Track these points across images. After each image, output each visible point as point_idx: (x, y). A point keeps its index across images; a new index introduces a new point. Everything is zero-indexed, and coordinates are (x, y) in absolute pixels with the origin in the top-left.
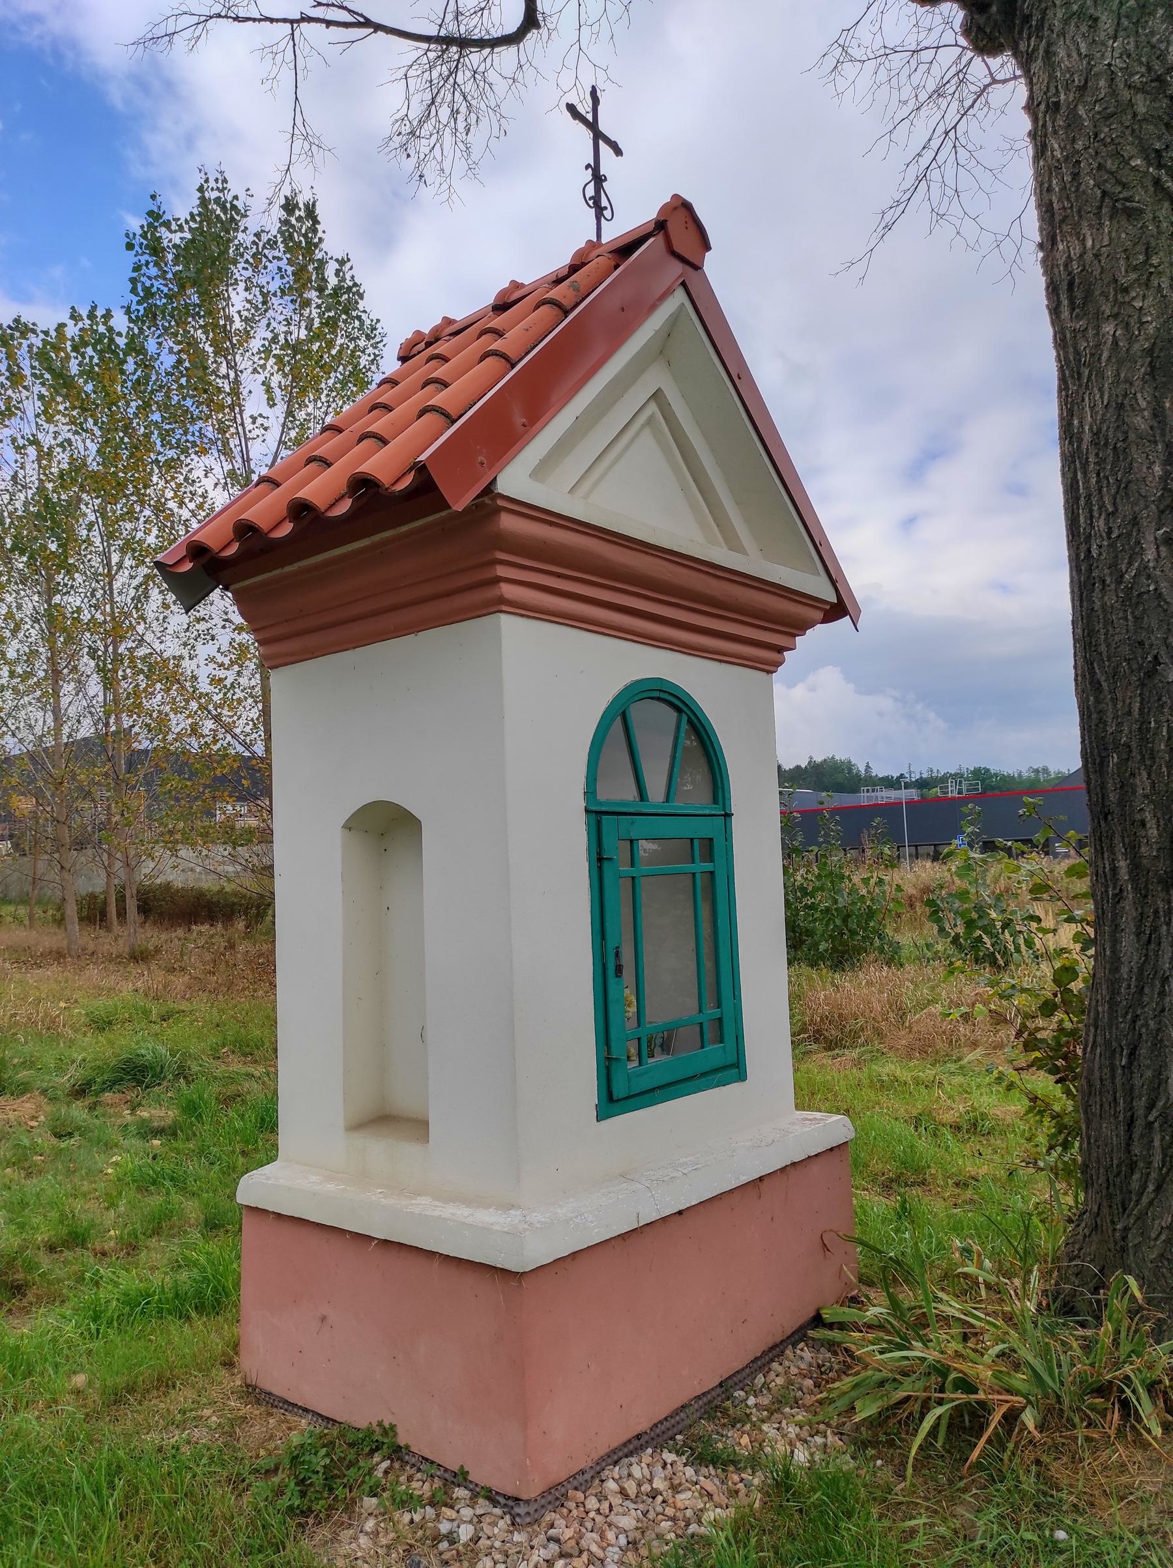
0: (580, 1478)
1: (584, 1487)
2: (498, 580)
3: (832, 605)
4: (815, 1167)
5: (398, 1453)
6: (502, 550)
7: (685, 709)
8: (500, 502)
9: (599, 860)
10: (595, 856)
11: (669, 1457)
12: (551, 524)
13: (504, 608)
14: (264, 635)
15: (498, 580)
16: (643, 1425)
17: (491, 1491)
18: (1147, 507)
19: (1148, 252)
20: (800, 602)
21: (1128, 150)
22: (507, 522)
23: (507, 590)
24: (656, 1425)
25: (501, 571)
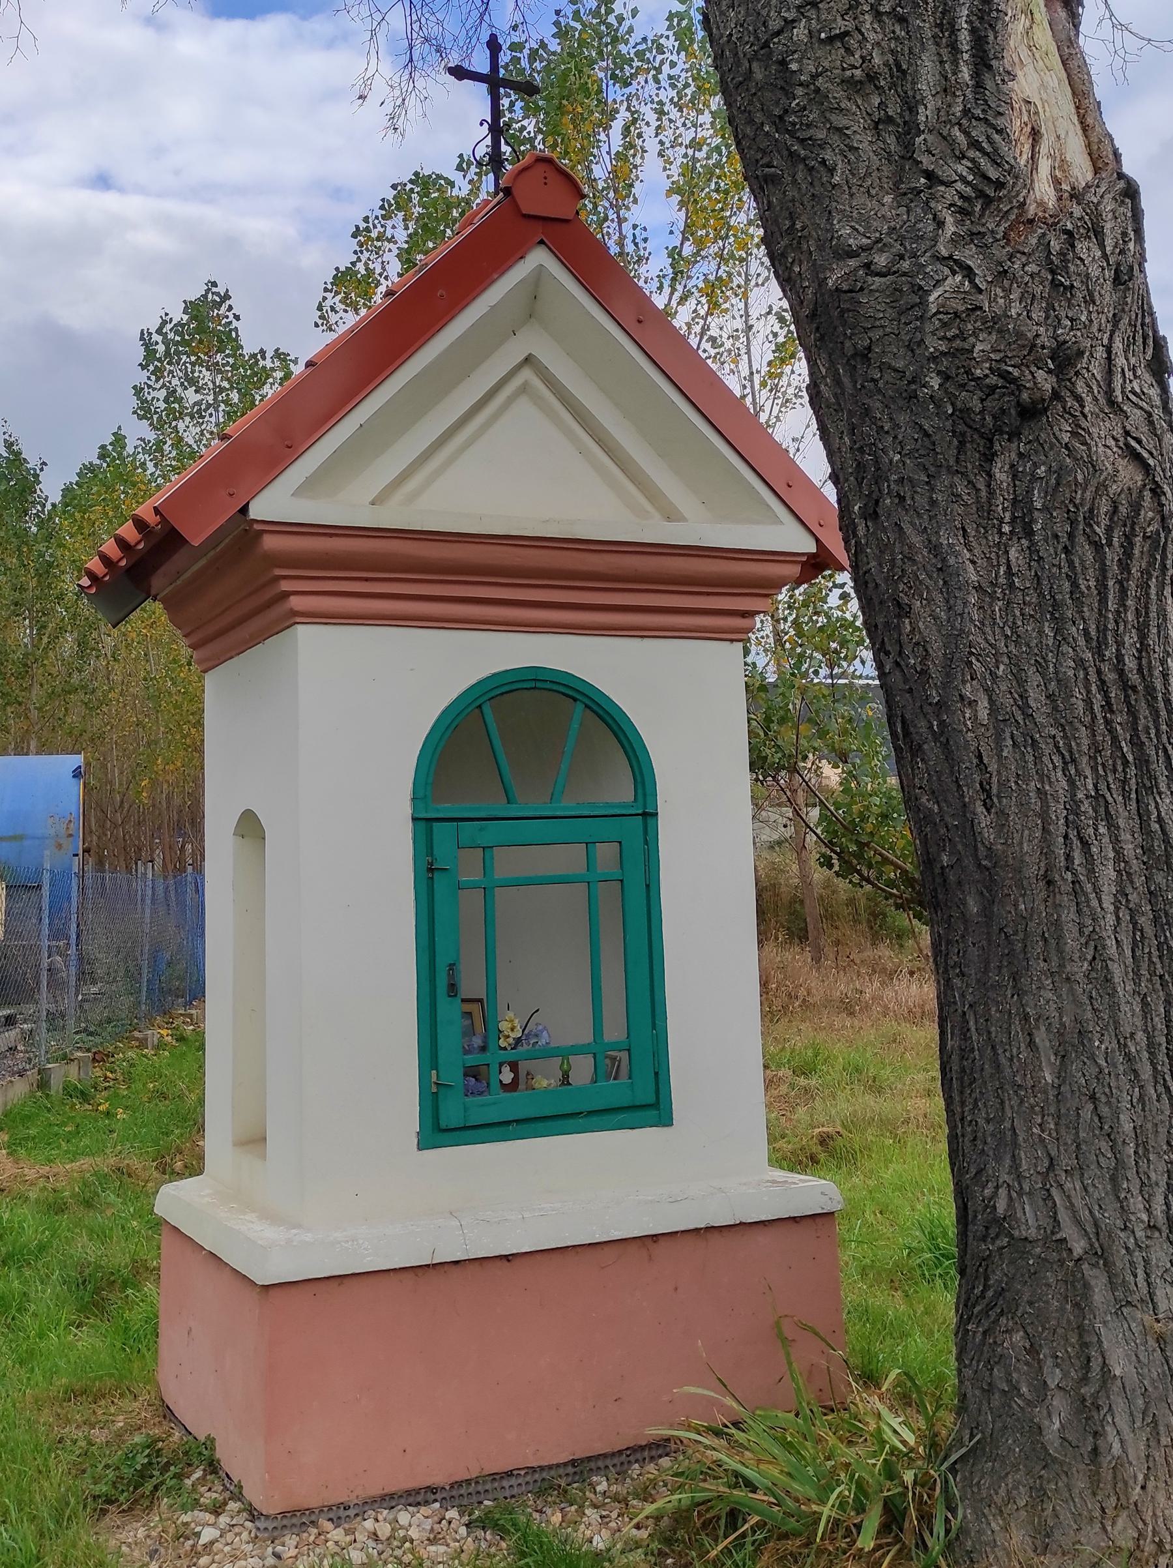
0: (342, 1513)
1: (337, 1522)
2: (286, 595)
3: (811, 556)
4: (762, 1238)
5: (213, 1467)
6: (280, 567)
7: (578, 697)
8: (256, 527)
9: (429, 871)
10: (425, 866)
11: (452, 1514)
12: (331, 535)
13: (298, 620)
14: (195, 638)
15: (286, 595)
16: (438, 1479)
17: (251, 1505)
18: (847, 480)
19: (792, 217)
20: (734, 559)
21: (759, 117)
22: (270, 543)
23: (295, 602)
24: (459, 1484)
25: (285, 586)
